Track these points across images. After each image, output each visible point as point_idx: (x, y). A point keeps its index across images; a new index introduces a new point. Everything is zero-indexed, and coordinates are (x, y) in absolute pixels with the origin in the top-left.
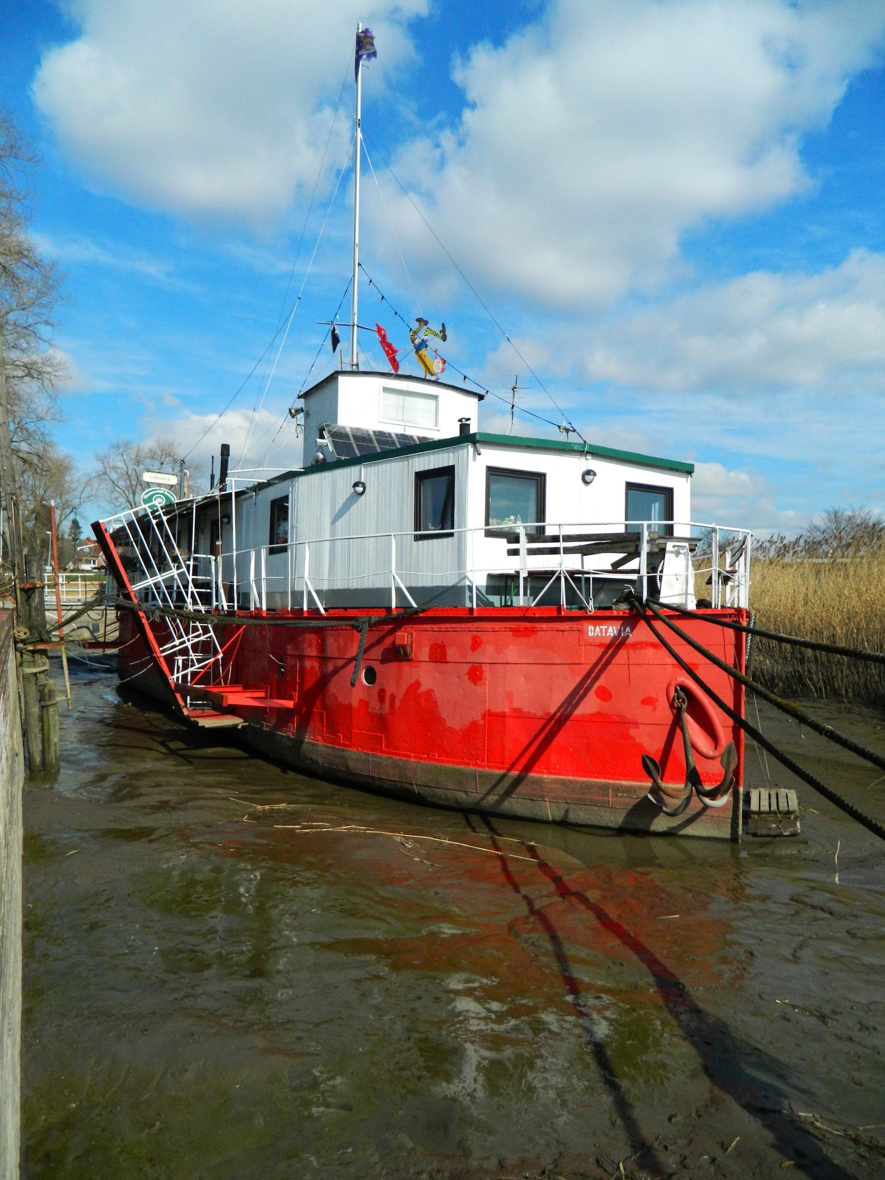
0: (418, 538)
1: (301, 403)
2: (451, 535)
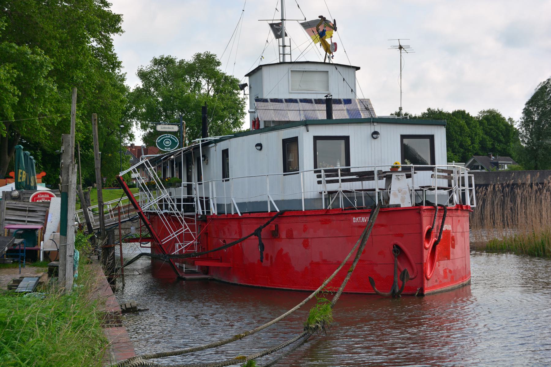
0: (284, 175)
2: (298, 173)
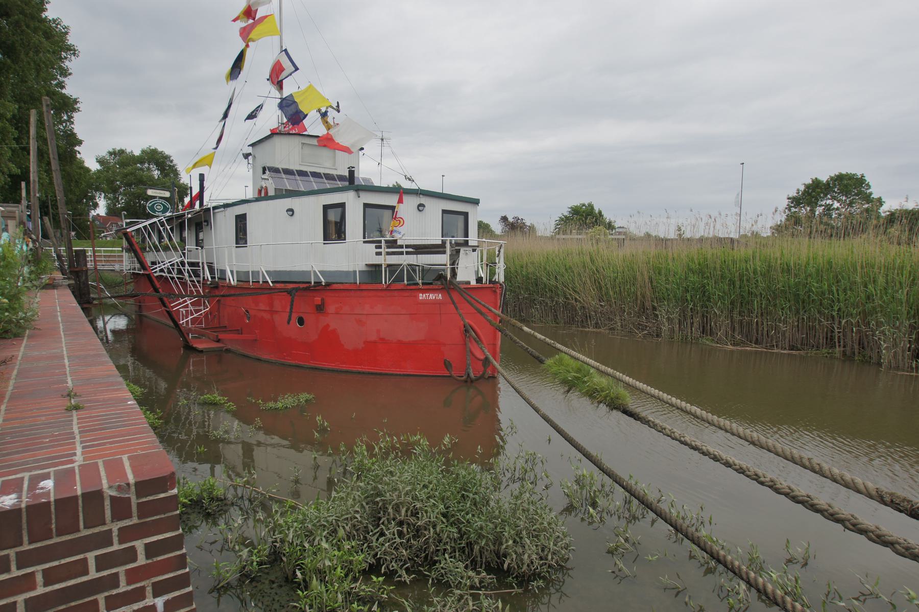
1: (250, 150)
